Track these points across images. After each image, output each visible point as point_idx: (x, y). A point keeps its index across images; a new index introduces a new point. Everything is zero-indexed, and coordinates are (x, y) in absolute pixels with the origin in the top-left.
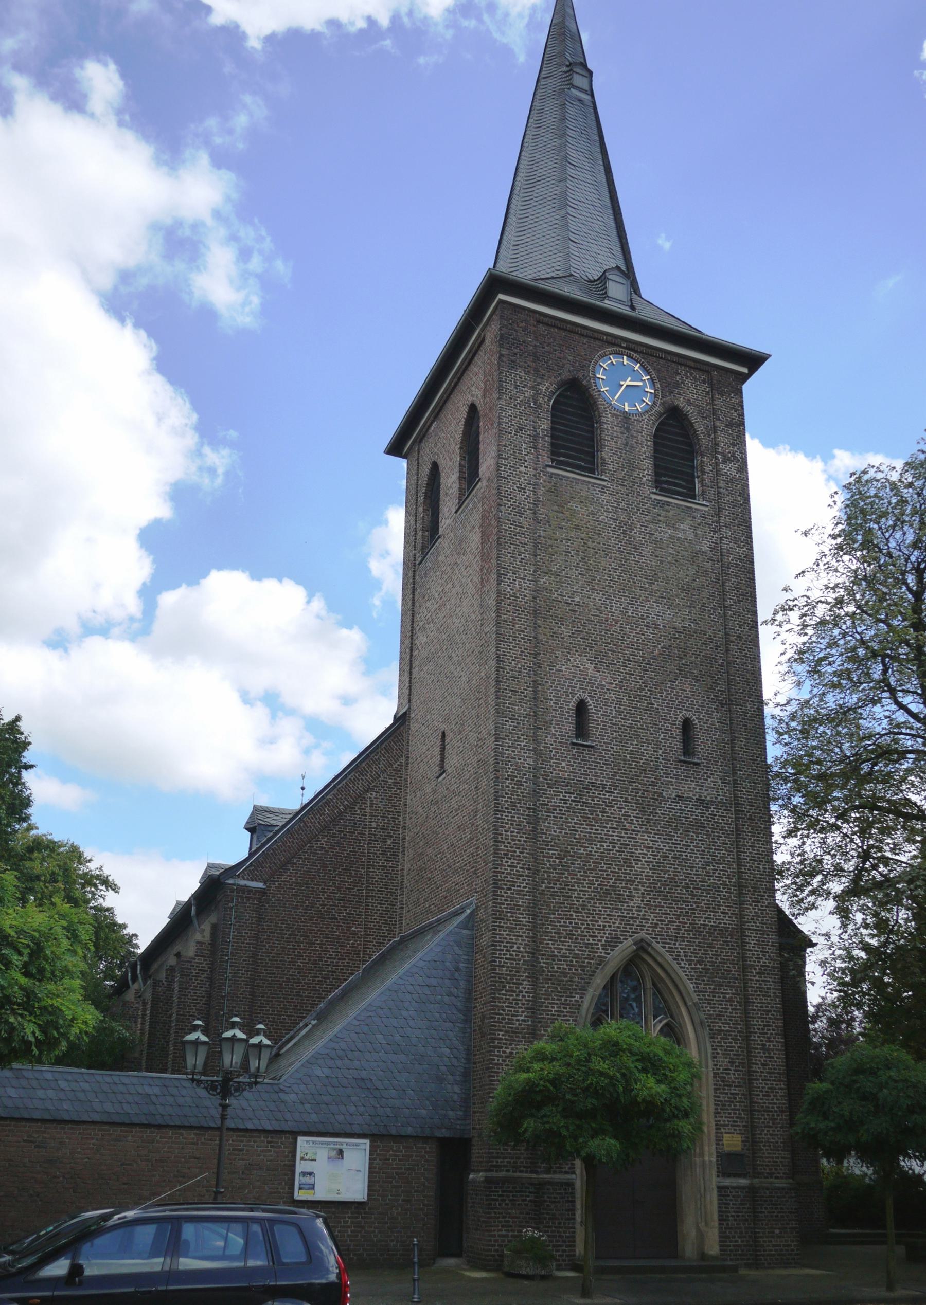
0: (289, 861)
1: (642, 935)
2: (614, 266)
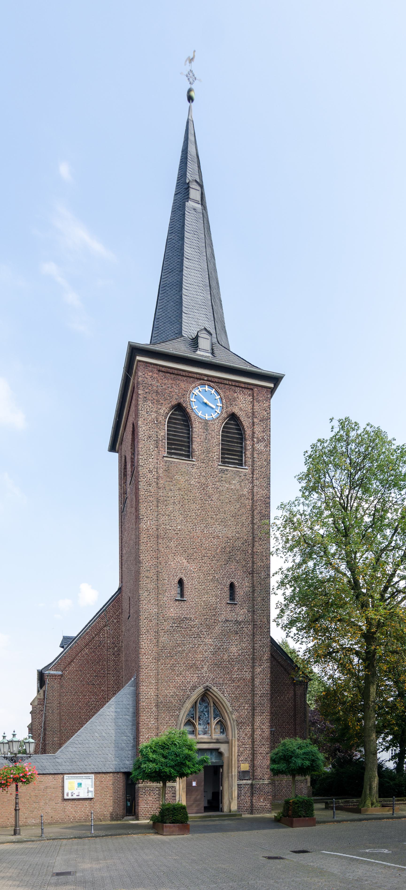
0: (72, 661)
1: (207, 684)
2: (203, 328)
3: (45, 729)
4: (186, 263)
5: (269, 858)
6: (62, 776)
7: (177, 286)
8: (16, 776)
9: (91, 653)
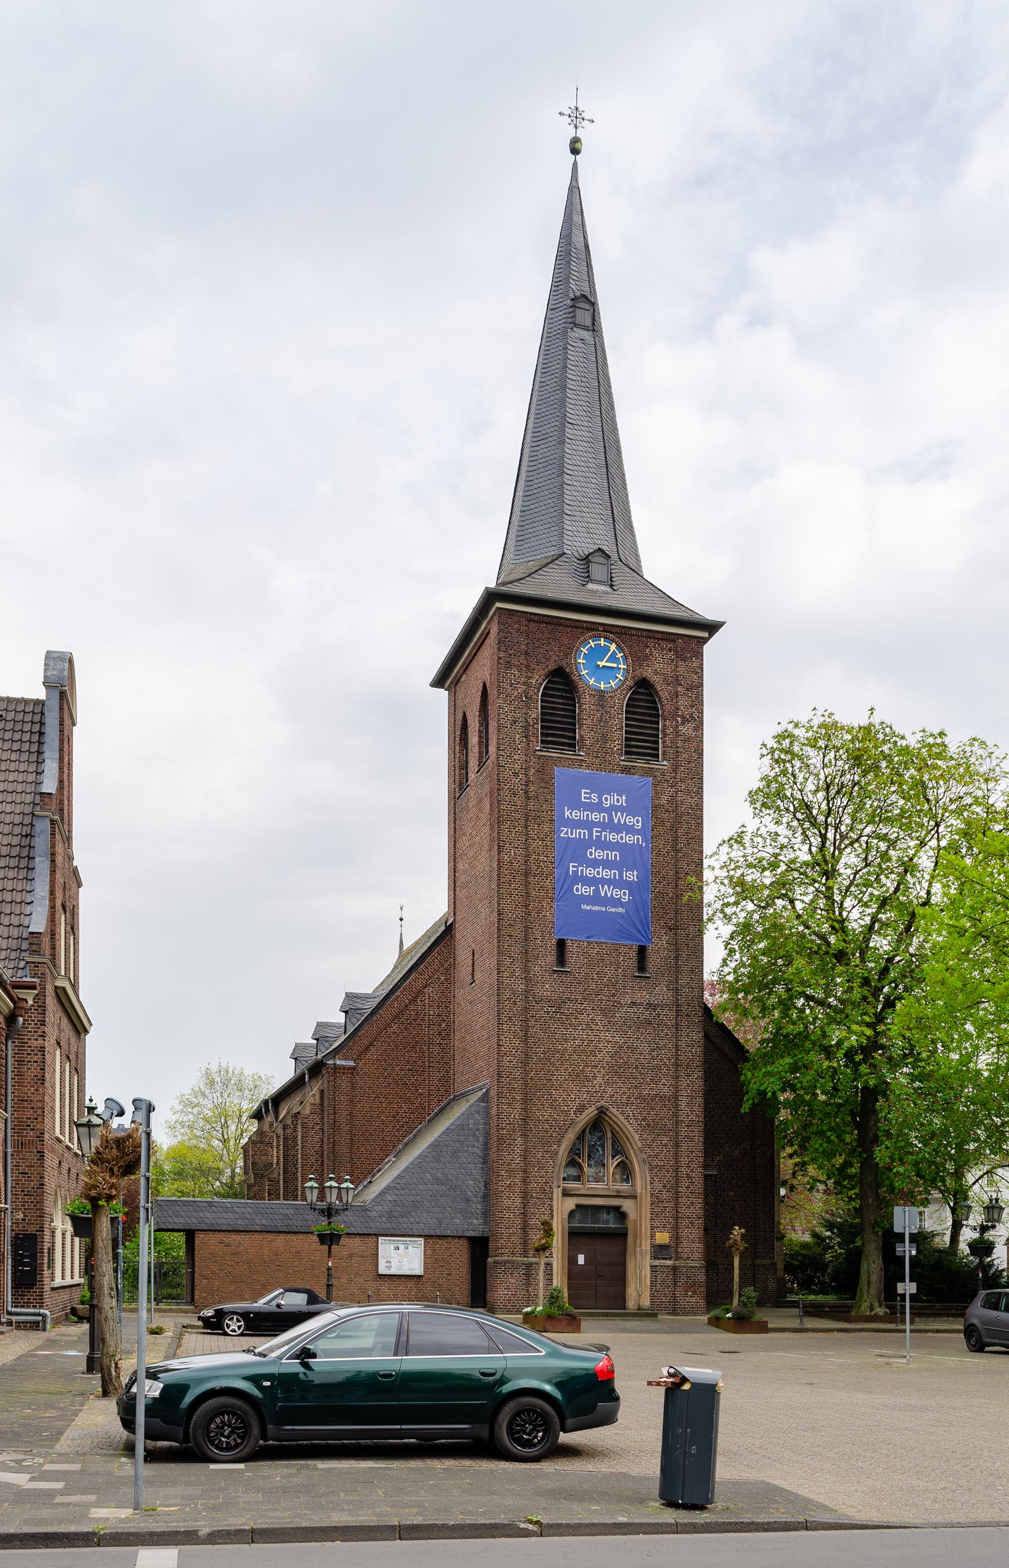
0: (371, 1044)
1: (602, 1103)
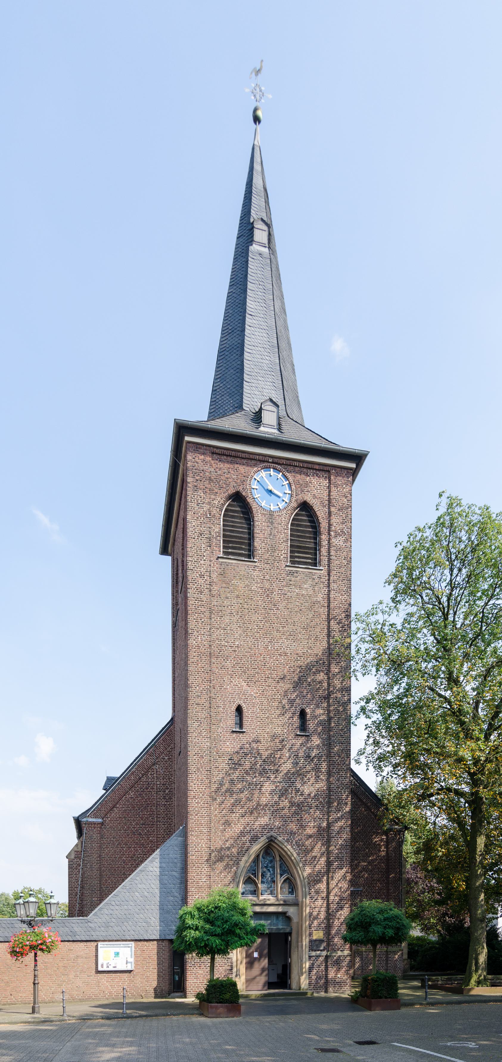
1: (272, 833)
3: (82, 887)
4: (248, 320)
5: (323, 1050)
6: (96, 944)
7: (238, 349)
8: (32, 943)
9: (137, 797)
